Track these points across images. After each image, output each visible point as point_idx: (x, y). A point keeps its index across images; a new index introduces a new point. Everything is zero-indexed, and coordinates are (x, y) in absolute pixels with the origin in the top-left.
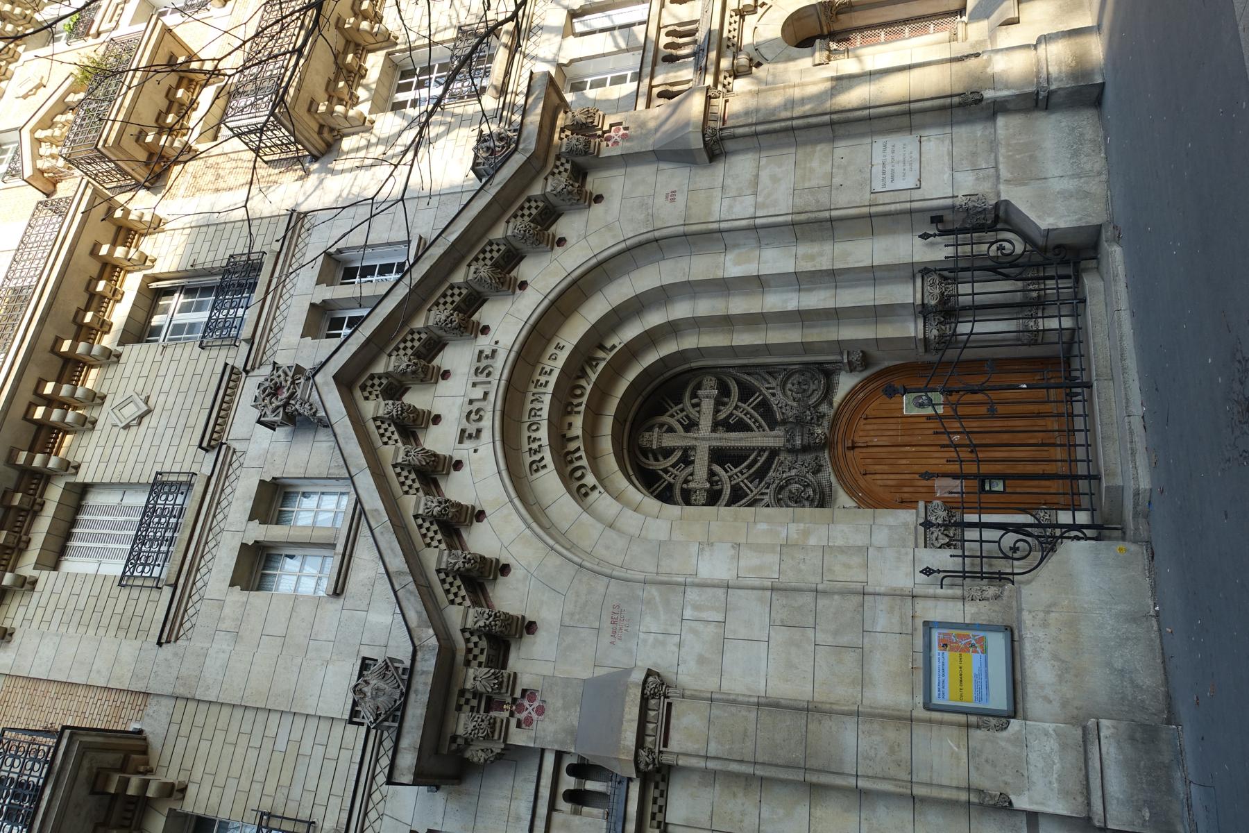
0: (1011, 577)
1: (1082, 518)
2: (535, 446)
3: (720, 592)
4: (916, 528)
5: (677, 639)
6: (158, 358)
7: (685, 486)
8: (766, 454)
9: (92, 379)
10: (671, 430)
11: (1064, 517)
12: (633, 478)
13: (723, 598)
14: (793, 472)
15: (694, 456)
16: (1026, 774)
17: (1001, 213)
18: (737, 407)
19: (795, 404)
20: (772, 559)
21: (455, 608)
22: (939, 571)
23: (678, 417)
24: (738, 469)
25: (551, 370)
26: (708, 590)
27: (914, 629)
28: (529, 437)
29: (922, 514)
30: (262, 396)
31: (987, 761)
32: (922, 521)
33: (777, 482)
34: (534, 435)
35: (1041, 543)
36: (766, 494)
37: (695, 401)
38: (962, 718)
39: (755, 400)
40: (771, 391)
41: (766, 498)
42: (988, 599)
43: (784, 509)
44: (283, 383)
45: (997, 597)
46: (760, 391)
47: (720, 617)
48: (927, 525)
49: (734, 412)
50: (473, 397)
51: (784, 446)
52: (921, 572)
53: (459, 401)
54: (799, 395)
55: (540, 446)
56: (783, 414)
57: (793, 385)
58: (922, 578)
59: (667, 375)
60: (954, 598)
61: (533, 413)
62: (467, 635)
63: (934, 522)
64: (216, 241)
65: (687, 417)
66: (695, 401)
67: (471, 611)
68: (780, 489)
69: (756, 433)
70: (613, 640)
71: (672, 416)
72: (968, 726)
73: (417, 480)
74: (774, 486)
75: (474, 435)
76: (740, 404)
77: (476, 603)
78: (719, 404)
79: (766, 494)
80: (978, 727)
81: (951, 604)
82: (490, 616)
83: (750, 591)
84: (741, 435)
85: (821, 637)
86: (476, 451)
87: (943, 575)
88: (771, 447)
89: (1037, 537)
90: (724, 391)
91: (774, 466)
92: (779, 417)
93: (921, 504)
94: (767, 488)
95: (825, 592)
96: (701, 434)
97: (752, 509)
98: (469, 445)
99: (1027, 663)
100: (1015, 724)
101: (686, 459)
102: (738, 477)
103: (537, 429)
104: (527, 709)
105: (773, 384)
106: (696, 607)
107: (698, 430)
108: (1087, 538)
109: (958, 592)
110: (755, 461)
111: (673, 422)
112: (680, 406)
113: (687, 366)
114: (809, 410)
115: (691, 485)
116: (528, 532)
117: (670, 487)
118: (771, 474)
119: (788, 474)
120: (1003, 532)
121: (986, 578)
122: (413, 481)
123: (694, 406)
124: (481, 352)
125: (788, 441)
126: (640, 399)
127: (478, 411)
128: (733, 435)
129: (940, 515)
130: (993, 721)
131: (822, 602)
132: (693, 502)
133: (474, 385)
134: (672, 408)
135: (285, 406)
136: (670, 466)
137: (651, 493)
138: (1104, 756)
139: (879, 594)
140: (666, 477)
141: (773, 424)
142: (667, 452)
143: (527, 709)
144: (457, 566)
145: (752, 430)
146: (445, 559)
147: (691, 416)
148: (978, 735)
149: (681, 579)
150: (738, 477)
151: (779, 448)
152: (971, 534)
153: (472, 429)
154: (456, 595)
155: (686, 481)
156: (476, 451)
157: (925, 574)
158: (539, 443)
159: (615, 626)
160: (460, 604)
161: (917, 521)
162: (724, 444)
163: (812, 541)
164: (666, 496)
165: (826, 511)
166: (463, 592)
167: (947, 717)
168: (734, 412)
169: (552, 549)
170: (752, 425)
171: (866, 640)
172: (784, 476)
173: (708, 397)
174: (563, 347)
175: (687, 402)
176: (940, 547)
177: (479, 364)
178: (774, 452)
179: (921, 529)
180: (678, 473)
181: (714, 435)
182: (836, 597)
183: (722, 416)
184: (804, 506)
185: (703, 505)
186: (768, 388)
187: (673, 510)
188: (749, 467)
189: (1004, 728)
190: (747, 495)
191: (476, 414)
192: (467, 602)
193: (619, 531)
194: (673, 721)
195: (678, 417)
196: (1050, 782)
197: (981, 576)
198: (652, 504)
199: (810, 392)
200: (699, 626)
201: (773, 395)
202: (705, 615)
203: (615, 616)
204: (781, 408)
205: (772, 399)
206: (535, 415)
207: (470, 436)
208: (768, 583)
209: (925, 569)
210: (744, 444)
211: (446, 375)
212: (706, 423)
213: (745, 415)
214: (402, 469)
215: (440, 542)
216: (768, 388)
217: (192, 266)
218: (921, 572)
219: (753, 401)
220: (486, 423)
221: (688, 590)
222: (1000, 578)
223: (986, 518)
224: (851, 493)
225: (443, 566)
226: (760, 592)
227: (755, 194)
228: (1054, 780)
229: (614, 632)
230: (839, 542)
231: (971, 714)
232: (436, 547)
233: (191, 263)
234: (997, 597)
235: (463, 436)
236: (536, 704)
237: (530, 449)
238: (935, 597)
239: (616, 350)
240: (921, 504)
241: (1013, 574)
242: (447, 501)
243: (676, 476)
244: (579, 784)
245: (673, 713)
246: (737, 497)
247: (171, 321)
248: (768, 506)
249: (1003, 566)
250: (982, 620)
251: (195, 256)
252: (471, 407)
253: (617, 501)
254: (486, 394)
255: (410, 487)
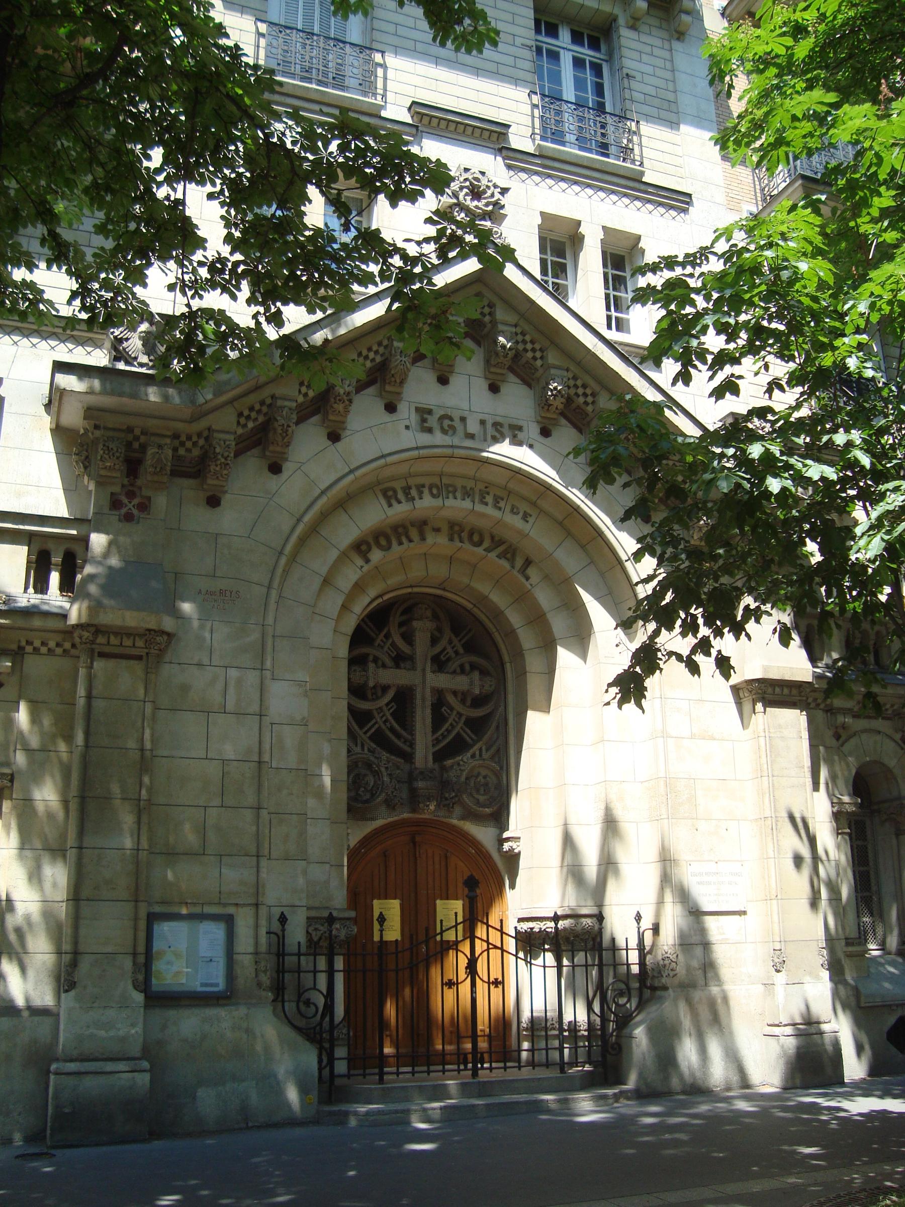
0: (280, 998)
1: (341, 1067)
2: (414, 492)
3: (255, 708)
4: (327, 908)
5: (206, 661)
6: (519, 41)
7: (371, 658)
8: (407, 748)
9: (432, 231)
10: (434, 641)
11: (341, 1052)
12: (380, 600)
13: (250, 711)
14: (385, 779)
15: (405, 668)
16: (94, 1005)
17: (658, 993)
18: (460, 715)
19: (463, 779)
20: (292, 761)
21: (233, 418)
22: (283, 930)
23: (449, 650)
24: (390, 718)
25: (500, 509)
26: (258, 695)
27: (225, 905)
28: (423, 486)
29: (342, 915)
30: (470, 178)
31: (104, 971)
32: (335, 914)
33: (376, 761)
34: (426, 491)
35: (314, 1028)
36: (363, 749)
37: (467, 667)
38: (141, 949)
39: (468, 735)
40: (477, 753)
41: (358, 749)
42: (257, 976)
43: (346, 770)
44: (484, 201)
45: (259, 985)
46: (478, 741)
47: (230, 706)
48: (331, 920)
49: (455, 713)
50: (469, 422)
51: (416, 769)
52: (282, 913)
53: (465, 406)
54: (472, 784)
55: (413, 499)
56: (452, 766)
57: (485, 777)
58: (276, 912)
59: (496, 635)
60: (257, 944)
61: (450, 489)
62: (205, 434)
63: (333, 927)
64: (656, 102)
65: (449, 659)
66: (467, 667)
67: (232, 437)
68: (369, 765)
69: (430, 738)
70: (203, 592)
71: (450, 642)
72: (135, 954)
73: (374, 363)
74: (372, 758)
75: (425, 425)
76: (463, 719)
77: (239, 440)
78: (463, 696)
79: (363, 749)
80: (135, 963)
81: (251, 941)
82: (226, 459)
83: (257, 739)
84: (429, 720)
85: (213, 813)
86: (407, 427)
87: (280, 934)
88: (414, 753)
89: (320, 1024)
90: (478, 702)
91: (393, 757)
92: (449, 763)
93: (352, 914)
94: (369, 750)
95: (258, 816)
96: (430, 676)
97: (345, 736)
98: (414, 418)
99: (196, 1011)
100: (139, 997)
101: (400, 660)
102: (382, 717)
103: (433, 496)
104: (130, 502)
105: (486, 755)
106: (239, 682)
107: (434, 672)
108: (320, 1069)
109: (263, 948)
110: (399, 736)
111: (443, 643)
112: (461, 651)
113: (506, 658)
114: (456, 796)
115: (371, 666)
116: (317, 492)
117: (370, 641)
118: (385, 755)
119: (385, 774)
120: (325, 993)
121: (279, 959)
122: (373, 360)
123: (462, 666)
124: (520, 428)
125: (422, 773)
126: (469, 606)
127: (451, 427)
128: (428, 711)
129: (340, 932)
130: (141, 977)
131: (249, 815)
132: (353, 668)
133: (483, 422)
134: (460, 641)
135: (458, 204)
136: (393, 642)
137: (363, 620)
138: (117, 1075)
139: (258, 871)
140: (381, 636)
141: (439, 757)
142: (408, 638)
143: (130, 502)
144: (279, 418)
145: (434, 732)
146: (287, 403)
147: (450, 663)
148: (128, 963)
149: (268, 664)
150: (382, 717)
151: (414, 763)
152: (322, 963)
153: (432, 421)
154: (248, 417)
155: (376, 660)
156: (407, 427)
157: (280, 917)
158: (417, 497)
159: (218, 593)
160: (238, 423)
161: (335, 909)
162: (418, 702)
163: (311, 802)
164: (359, 638)
165: (344, 815)
166: (251, 425)
167: (142, 935)
168: (455, 713)
169: (299, 520)
170: (440, 733)
171: (212, 858)
172: (383, 769)
173: (471, 683)
174: (527, 522)
175: (467, 659)
176: (307, 932)
177: (506, 426)
178: (408, 757)
179: (325, 914)
180: (386, 649)
181: (428, 691)
182: (254, 828)
183: (451, 699)
184: (349, 790)
185: (349, 679)
186: (480, 750)
187: (343, 651)
188: (392, 729)
189: (136, 987)
190: (361, 728)
191: (449, 426)
192: (240, 431)
193: (321, 590)
194: (124, 662)
195: (449, 650)
196: (88, 1027)
197: (280, 970)
198: (350, 623)
199: (476, 796)
200: (220, 686)
201: (473, 756)
202: (231, 691)
203: (228, 594)
204: (459, 764)
205: (469, 755)
206: (449, 492)
207: (424, 420)
208: (266, 758)
209: (285, 917)
210: (418, 726)
211: (494, 388)
212: (442, 681)
213: (451, 725)
214: (386, 347)
215: (306, 395)
216: (480, 750)
217: (627, 75)
218: (282, 913)
219: (466, 733)
220: (438, 438)
221: (258, 673)
222: (279, 989)
223: (339, 979)
224: (366, 842)
225: (279, 403)
226: (257, 750)
227: (693, 737)
228: (91, 1031)
229: (212, 593)
230: (311, 830)
231: (147, 958)
232: (300, 392)
233: (631, 73)
234: (259, 985)
235: (424, 413)
236: (135, 512)
237: (410, 488)
238: (257, 926)
239: (523, 580)
240: (352, 914)
241: (283, 1001)
242: (350, 401)
243: (382, 647)
244: (57, 565)
245: (132, 662)
246: (358, 717)
247: (564, 48)
248: (349, 751)
249: (290, 994)
250: (238, 971)
251: (639, 76)
252: (457, 419)
253: (354, 586)
254: (472, 436)
255: (366, 357)
